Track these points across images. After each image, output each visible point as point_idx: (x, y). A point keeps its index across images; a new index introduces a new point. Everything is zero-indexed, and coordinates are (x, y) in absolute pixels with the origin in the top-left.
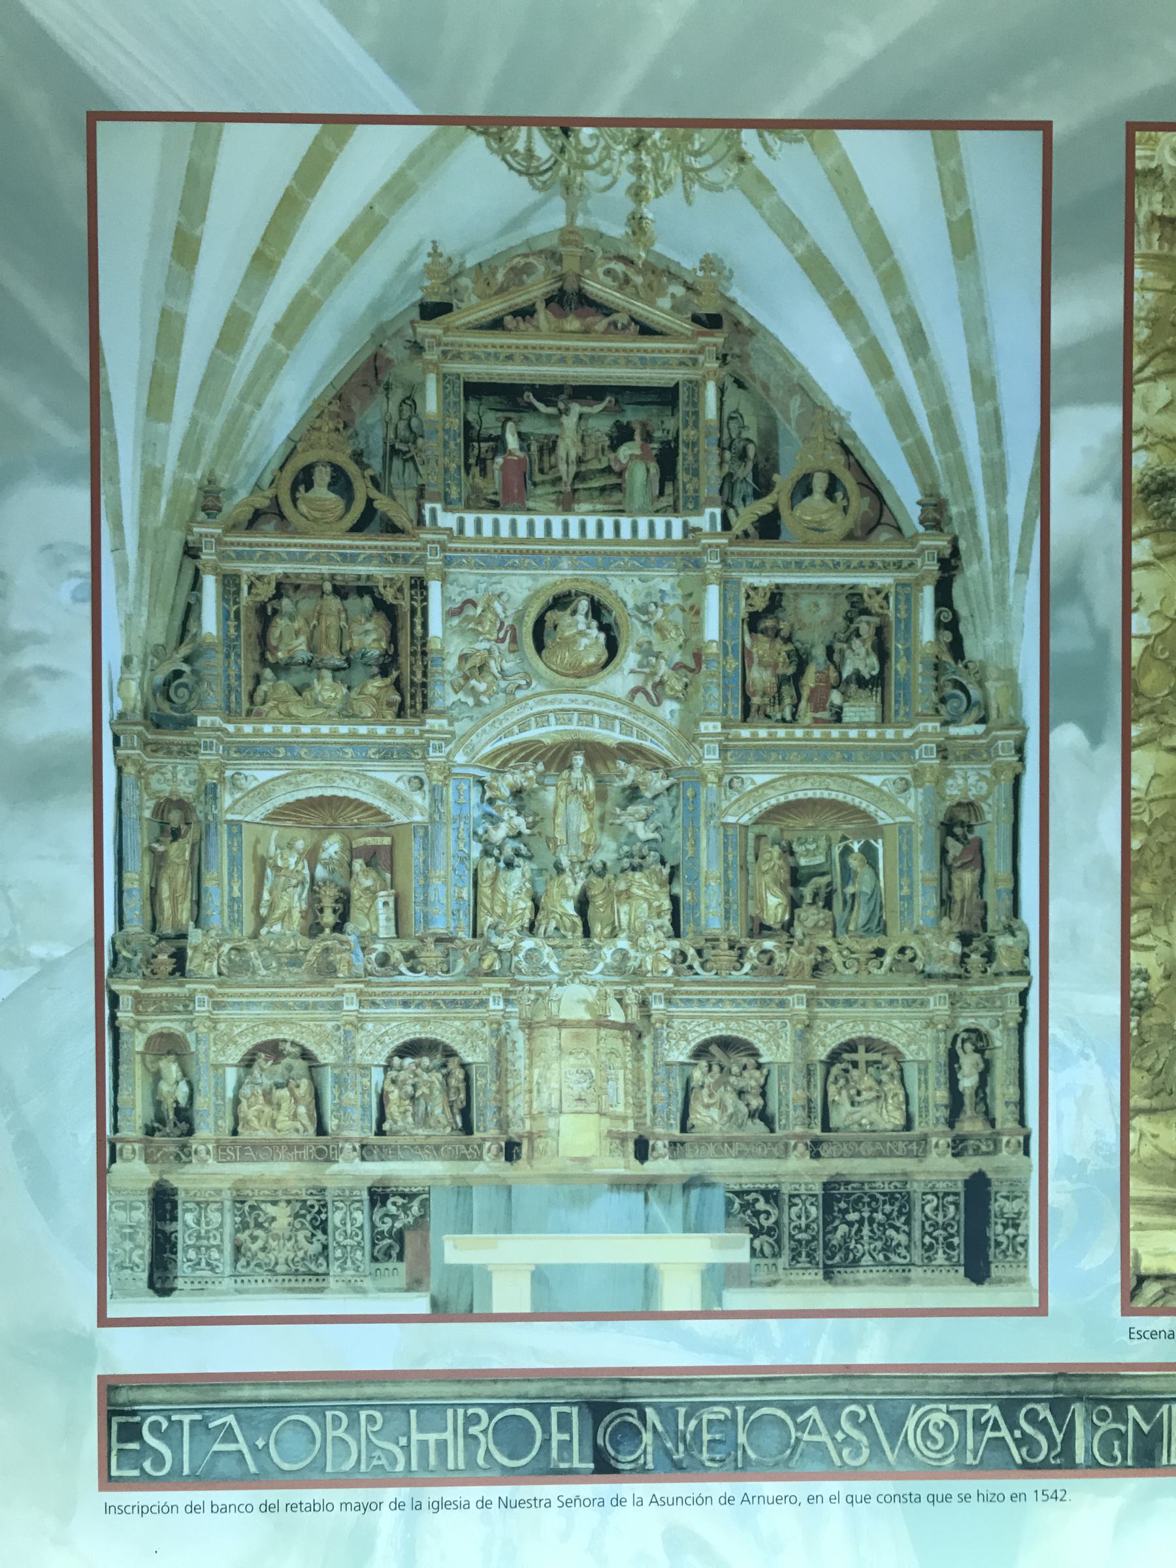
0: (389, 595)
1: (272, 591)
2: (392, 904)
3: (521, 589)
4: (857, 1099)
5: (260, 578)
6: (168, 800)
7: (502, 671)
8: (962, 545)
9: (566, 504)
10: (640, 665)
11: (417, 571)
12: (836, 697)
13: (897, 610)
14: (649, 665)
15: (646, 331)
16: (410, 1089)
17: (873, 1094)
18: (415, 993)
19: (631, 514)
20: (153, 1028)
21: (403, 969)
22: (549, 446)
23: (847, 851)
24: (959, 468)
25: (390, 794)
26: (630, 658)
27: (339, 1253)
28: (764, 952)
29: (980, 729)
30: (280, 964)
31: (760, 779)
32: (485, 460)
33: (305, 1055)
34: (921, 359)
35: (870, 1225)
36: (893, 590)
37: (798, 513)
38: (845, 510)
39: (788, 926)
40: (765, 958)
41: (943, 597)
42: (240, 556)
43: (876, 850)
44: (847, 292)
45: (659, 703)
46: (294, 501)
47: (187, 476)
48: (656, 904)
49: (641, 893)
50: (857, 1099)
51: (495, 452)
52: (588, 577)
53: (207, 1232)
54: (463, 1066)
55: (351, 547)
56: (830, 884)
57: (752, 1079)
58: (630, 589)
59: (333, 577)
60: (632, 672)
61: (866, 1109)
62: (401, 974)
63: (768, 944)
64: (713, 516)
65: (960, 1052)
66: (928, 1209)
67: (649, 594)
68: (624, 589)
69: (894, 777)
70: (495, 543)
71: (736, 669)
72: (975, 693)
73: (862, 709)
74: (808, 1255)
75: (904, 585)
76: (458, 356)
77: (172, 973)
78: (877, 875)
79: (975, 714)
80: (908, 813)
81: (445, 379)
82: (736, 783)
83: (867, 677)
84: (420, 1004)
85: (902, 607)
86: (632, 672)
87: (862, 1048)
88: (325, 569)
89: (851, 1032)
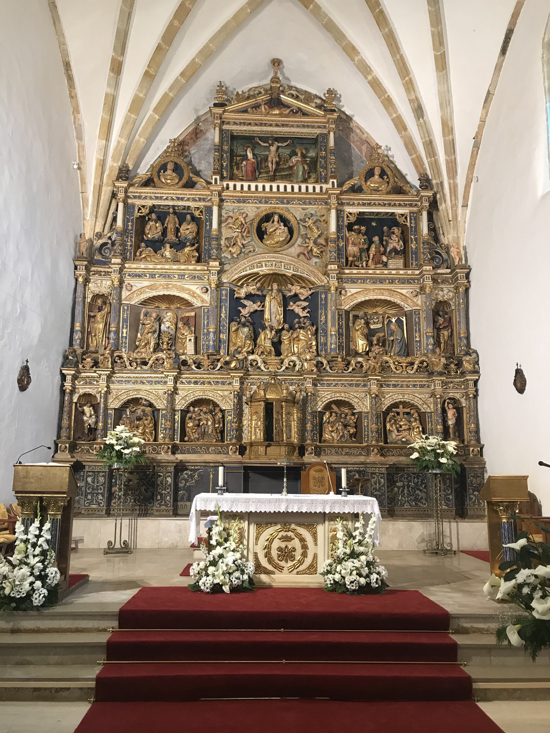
0: (197, 214)
1: (147, 211)
2: (193, 340)
3: (253, 211)
4: (400, 429)
5: (143, 206)
6: (97, 294)
7: (243, 245)
9: (273, 179)
10: (302, 243)
11: (209, 204)
12: (384, 259)
13: (411, 223)
14: (306, 243)
17: (407, 427)
18: (200, 378)
21: (193, 367)
23: (390, 322)
24: (435, 165)
25: (193, 294)
28: (359, 362)
29: (449, 271)
30: (137, 365)
31: (353, 291)
32: (238, 164)
33: (151, 405)
34: (421, 119)
35: (408, 488)
36: (408, 215)
38: (388, 183)
39: (367, 353)
40: (358, 365)
41: (430, 218)
43: (403, 321)
44: (389, 96)
45: (310, 259)
49: (303, 338)
50: (400, 429)
52: (280, 208)
53: (97, 486)
54: (222, 411)
56: (384, 336)
57: (352, 420)
59: (173, 207)
60: (299, 246)
62: (192, 369)
63: (360, 359)
64: (333, 183)
65: (447, 408)
67: (306, 215)
68: (295, 212)
69: (412, 290)
70: (242, 193)
71: (343, 245)
72: (445, 256)
73: (396, 263)
75: (413, 213)
77: (92, 367)
78: (403, 332)
80: (418, 305)
82: (343, 292)
83: (399, 250)
84: (203, 383)
85: (413, 221)
86: (299, 246)
87: (401, 406)
88: (171, 203)
89: (399, 398)
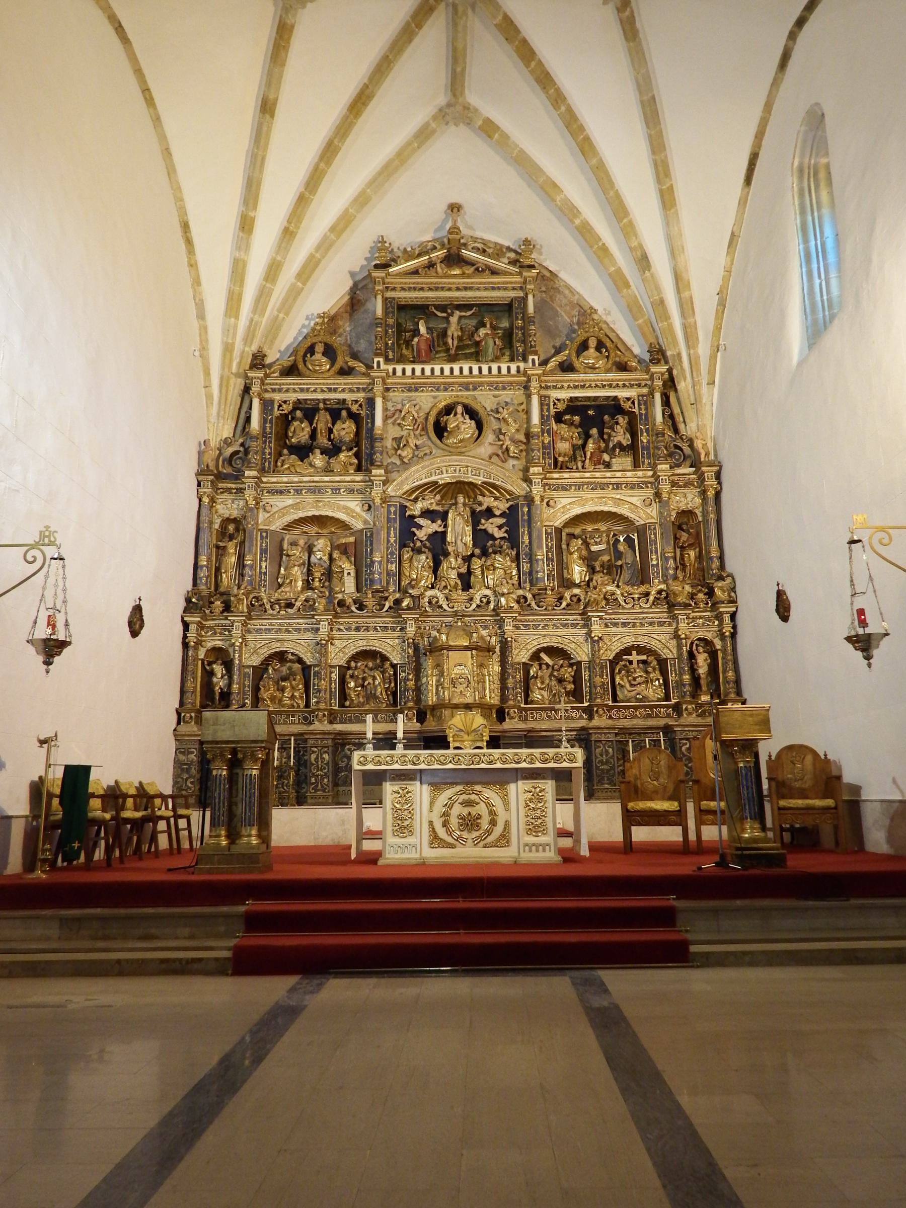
3: (428, 402)
6: (228, 519)
8: (675, 372)
9: (452, 359)
12: (606, 457)
13: (640, 409)
15: (494, 272)
16: (360, 681)
19: (487, 362)
20: (210, 645)
22: (444, 334)
26: (489, 437)
27: (313, 780)
37: (581, 359)
38: (607, 357)
41: (666, 403)
42: (274, 390)
46: (305, 362)
47: (247, 349)
48: (508, 572)
51: (414, 336)
52: (465, 396)
55: (334, 384)
58: (488, 401)
59: (324, 400)
61: (639, 689)
65: (695, 652)
66: (683, 749)
68: (485, 400)
74: (608, 779)
75: (643, 396)
76: (394, 289)
79: (688, 462)
81: (385, 300)
82: (552, 503)
85: (643, 407)
87: (634, 653)
88: (320, 396)
